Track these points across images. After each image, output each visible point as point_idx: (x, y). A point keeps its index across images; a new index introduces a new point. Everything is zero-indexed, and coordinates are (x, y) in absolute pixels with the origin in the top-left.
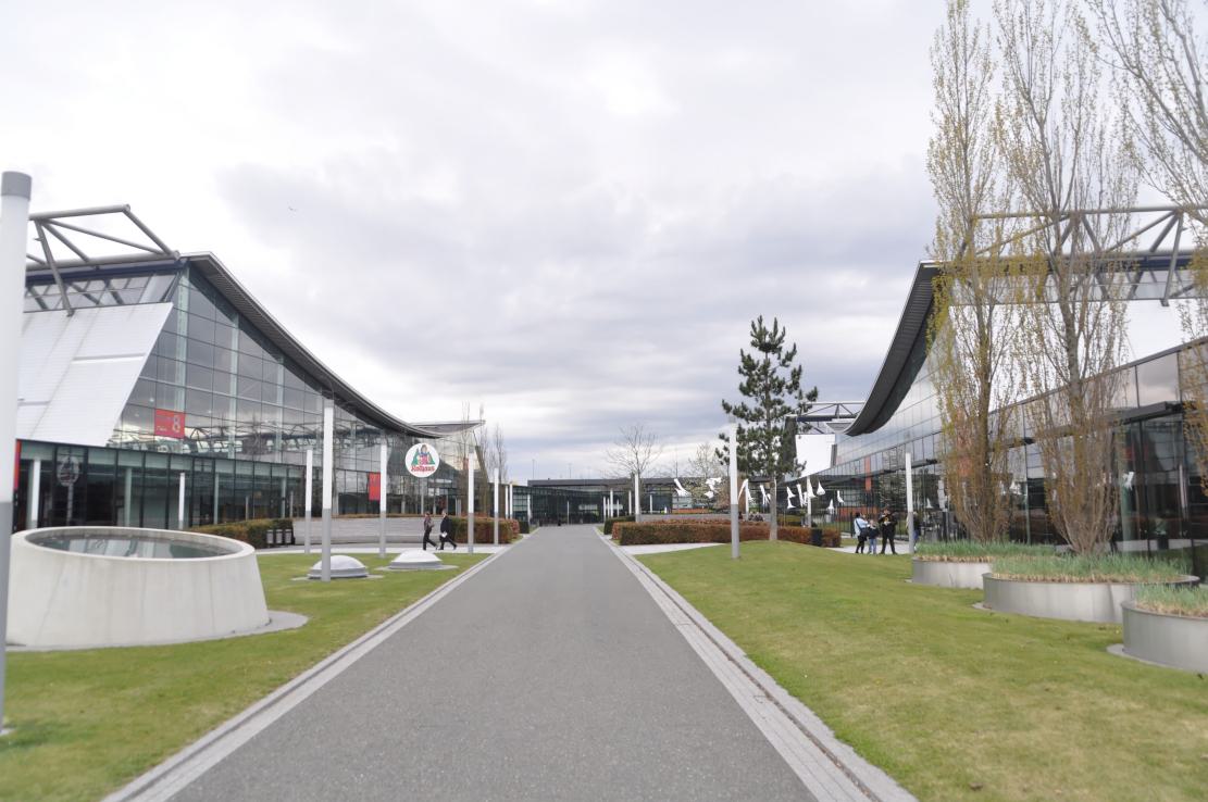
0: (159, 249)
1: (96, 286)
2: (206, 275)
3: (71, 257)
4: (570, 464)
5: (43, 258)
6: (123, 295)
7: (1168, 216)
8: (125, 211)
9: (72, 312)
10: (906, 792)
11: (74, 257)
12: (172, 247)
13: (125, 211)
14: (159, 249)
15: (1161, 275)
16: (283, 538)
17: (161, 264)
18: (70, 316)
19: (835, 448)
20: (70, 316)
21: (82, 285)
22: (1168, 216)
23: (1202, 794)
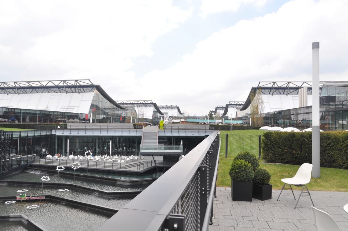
0: (42, 85)
1: (22, 90)
2: (98, 88)
3: (18, 86)
4: (311, 113)
5: (15, 86)
6: (38, 92)
7: (78, 82)
8: (89, 80)
9: (8, 94)
10: (334, 169)
11: (54, 85)
12: (94, 84)
13: (89, 80)
14: (42, 85)
15: (287, 90)
16: (139, 127)
17: (92, 86)
18: (79, 93)
19: (237, 112)
20: (79, 93)
21: (20, 89)
22: (78, 82)
23: (230, 180)
